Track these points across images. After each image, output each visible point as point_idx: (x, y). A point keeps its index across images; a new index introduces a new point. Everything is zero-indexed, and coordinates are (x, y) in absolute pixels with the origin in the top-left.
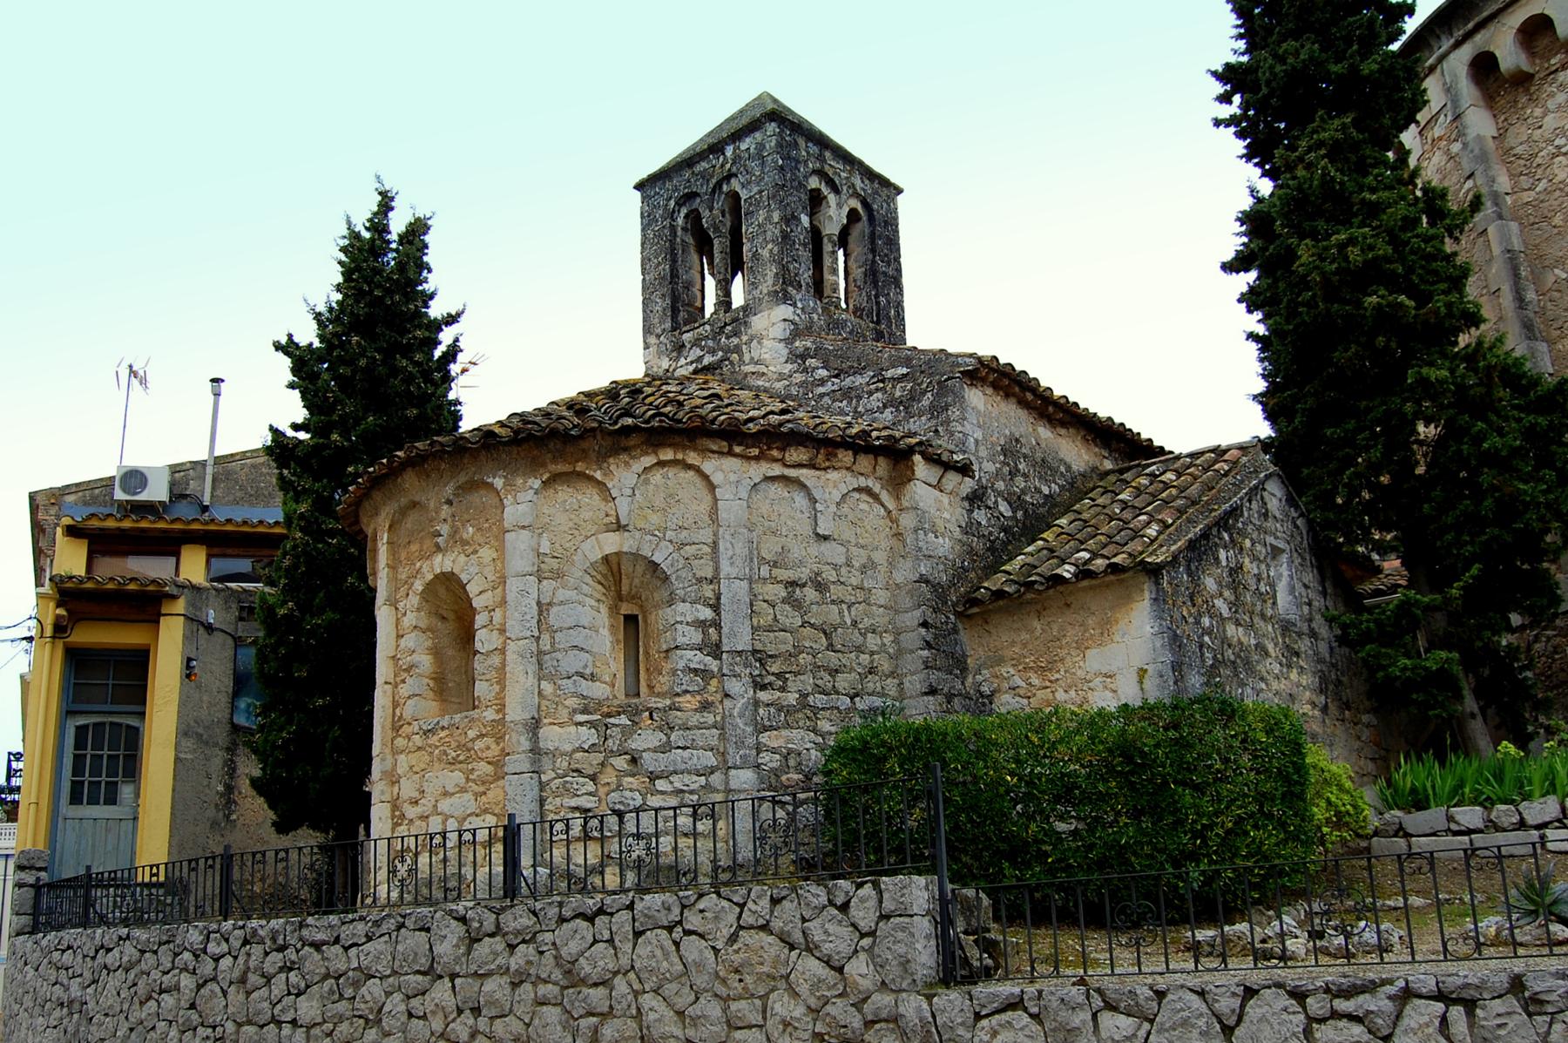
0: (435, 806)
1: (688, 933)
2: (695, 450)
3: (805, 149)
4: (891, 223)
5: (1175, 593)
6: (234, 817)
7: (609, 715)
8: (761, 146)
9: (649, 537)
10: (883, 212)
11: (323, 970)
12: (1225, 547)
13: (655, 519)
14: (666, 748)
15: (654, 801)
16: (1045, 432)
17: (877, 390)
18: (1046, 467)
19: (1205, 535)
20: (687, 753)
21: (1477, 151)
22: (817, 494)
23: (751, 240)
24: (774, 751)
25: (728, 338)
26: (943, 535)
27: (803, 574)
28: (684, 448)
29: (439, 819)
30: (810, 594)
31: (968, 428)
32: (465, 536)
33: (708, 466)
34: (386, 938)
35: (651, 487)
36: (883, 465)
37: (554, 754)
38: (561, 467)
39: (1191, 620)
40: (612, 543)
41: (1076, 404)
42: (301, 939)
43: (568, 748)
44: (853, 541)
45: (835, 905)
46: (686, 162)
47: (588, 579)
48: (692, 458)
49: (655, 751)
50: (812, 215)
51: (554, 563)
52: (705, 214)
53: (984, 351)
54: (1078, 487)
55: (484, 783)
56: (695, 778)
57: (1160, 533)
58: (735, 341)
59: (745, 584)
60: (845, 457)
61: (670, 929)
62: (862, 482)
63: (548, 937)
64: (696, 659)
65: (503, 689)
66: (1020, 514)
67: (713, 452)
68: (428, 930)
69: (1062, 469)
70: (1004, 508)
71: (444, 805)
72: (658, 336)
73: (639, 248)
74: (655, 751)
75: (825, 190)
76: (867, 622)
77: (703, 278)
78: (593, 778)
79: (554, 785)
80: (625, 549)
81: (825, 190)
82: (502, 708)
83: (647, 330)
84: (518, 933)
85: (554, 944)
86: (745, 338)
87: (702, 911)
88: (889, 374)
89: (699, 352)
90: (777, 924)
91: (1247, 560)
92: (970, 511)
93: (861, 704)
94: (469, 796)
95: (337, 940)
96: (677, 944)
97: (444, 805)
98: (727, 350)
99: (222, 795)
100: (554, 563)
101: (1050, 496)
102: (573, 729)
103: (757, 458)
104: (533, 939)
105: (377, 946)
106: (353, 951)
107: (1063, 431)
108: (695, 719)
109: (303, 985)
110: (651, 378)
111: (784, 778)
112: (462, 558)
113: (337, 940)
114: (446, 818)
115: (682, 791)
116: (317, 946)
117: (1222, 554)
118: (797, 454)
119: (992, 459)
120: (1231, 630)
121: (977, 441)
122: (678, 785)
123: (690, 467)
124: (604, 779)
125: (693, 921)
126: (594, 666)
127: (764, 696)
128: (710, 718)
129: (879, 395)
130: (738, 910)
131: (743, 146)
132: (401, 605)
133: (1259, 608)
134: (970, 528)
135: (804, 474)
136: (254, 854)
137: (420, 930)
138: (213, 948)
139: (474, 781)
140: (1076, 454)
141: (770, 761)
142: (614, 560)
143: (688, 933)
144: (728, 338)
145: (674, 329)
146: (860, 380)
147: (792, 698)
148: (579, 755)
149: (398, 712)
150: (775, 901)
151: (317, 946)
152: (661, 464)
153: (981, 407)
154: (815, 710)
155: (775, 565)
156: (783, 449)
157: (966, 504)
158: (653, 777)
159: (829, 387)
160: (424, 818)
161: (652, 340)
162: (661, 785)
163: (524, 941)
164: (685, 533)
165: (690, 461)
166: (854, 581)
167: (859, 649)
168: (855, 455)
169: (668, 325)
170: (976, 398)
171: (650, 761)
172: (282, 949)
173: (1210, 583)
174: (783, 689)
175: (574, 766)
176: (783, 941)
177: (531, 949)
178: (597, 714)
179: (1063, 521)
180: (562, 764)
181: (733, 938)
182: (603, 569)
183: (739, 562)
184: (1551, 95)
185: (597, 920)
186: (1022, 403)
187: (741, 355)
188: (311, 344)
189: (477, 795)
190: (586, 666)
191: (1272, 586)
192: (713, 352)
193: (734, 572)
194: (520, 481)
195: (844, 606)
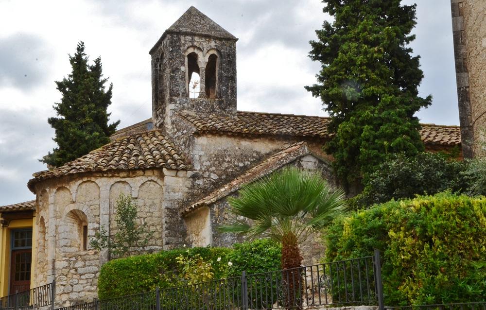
2: (94, 177)
13: (83, 199)
14: (84, 266)
20: (89, 268)
22: (131, 185)
28: (90, 177)
35: (82, 190)
36: (156, 173)
37: (58, 269)
38: (59, 185)
40: (72, 207)
44: (147, 197)
47: (68, 218)
48: (93, 179)
51: (59, 214)
56: (92, 275)
62: (150, 178)
74: (81, 267)
75: (196, 51)
76: (151, 223)
78: (66, 276)
81: (196, 51)
100: (59, 214)
108: (92, 257)
118: (122, 175)
122: (87, 277)
123: (93, 182)
124: (69, 276)
128: (96, 257)
135: (127, 180)
156: (118, 173)
158: (81, 275)
162: (83, 277)
164: (91, 202)
165: (92, 180)
166: (146, 210)
171: (80, 271)
178: (69, 258)
180: (60, 272)
183: (106, 209)
188: (327, 26)
193: (104, 213)
195: (142, 219)
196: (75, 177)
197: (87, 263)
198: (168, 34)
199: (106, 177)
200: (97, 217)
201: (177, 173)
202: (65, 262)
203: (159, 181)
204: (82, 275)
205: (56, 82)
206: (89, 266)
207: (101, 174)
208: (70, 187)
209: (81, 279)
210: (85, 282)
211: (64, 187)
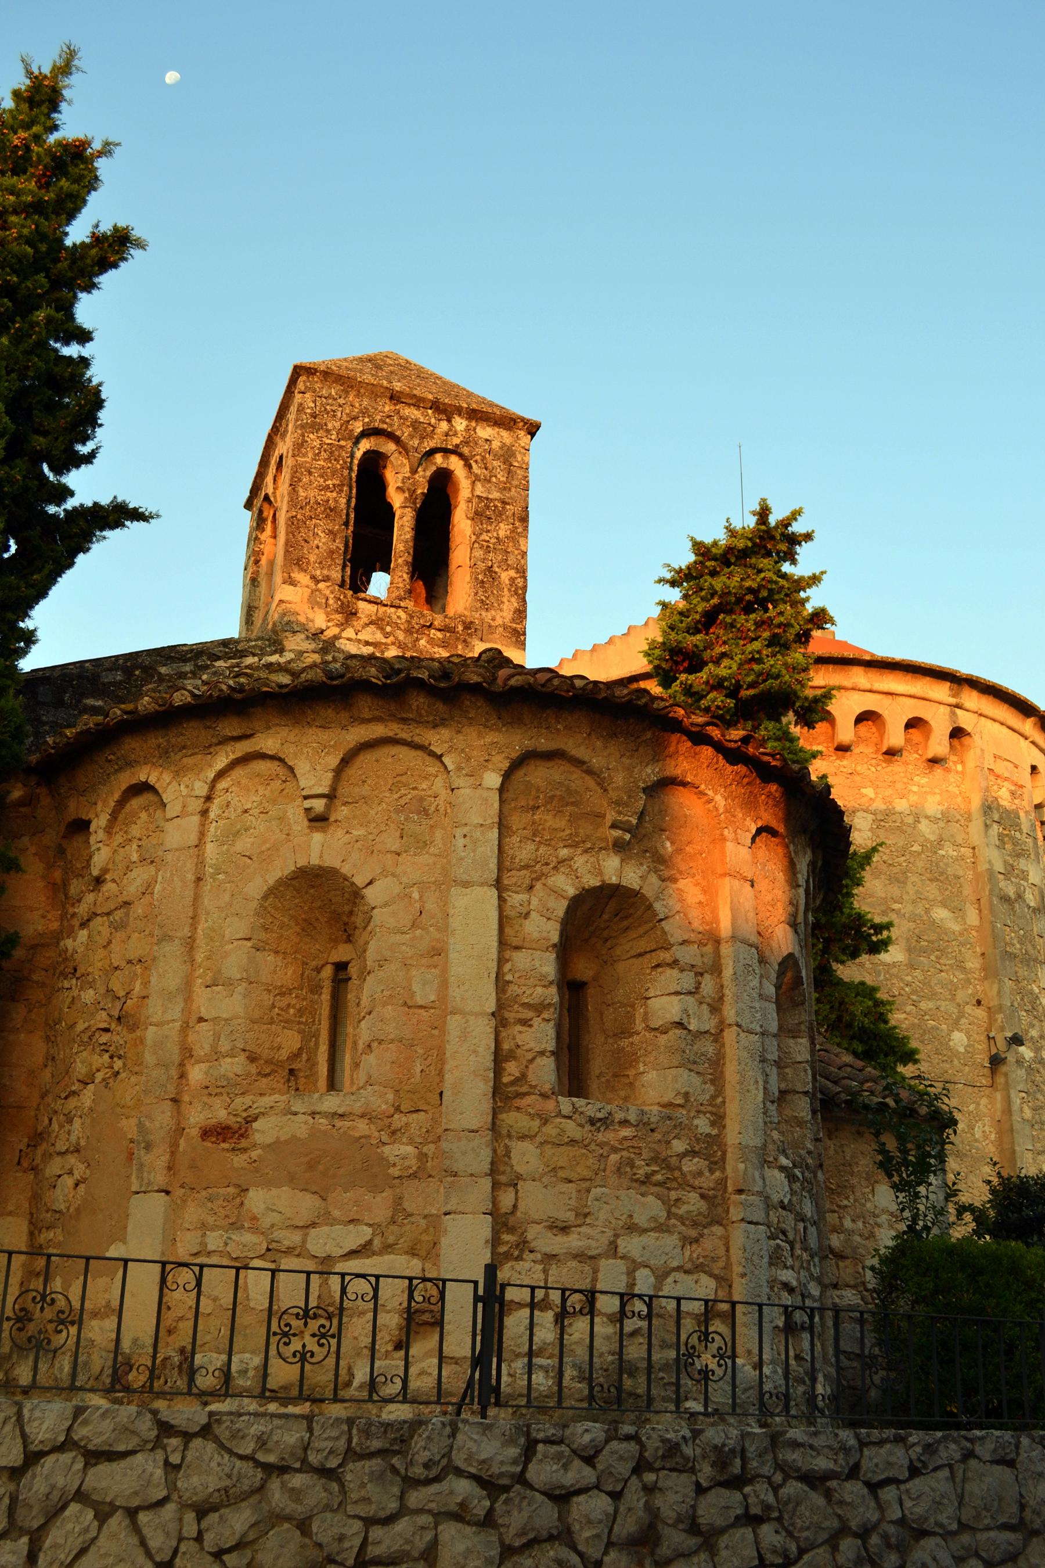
11: (836, 1524)
29: (621, 1266)
34: (945, 1473)
42: (778, 1466)
55: (695, 1224)
68: (1011, 1464)
71: (631, 1245)
82: (718, 1120)
95: (854, 1472)
105: (937, 1483)
106: (889, 1494)
109: (793, 1548)
113: (854, 1472)
114: (633, 1267)
116: (813, 1480)
137: (998, 1462)
138: (544, 1471)
139: (681, 1219)
151: (813, 1480)
172: (737, 1483)
189: (687, 1241)
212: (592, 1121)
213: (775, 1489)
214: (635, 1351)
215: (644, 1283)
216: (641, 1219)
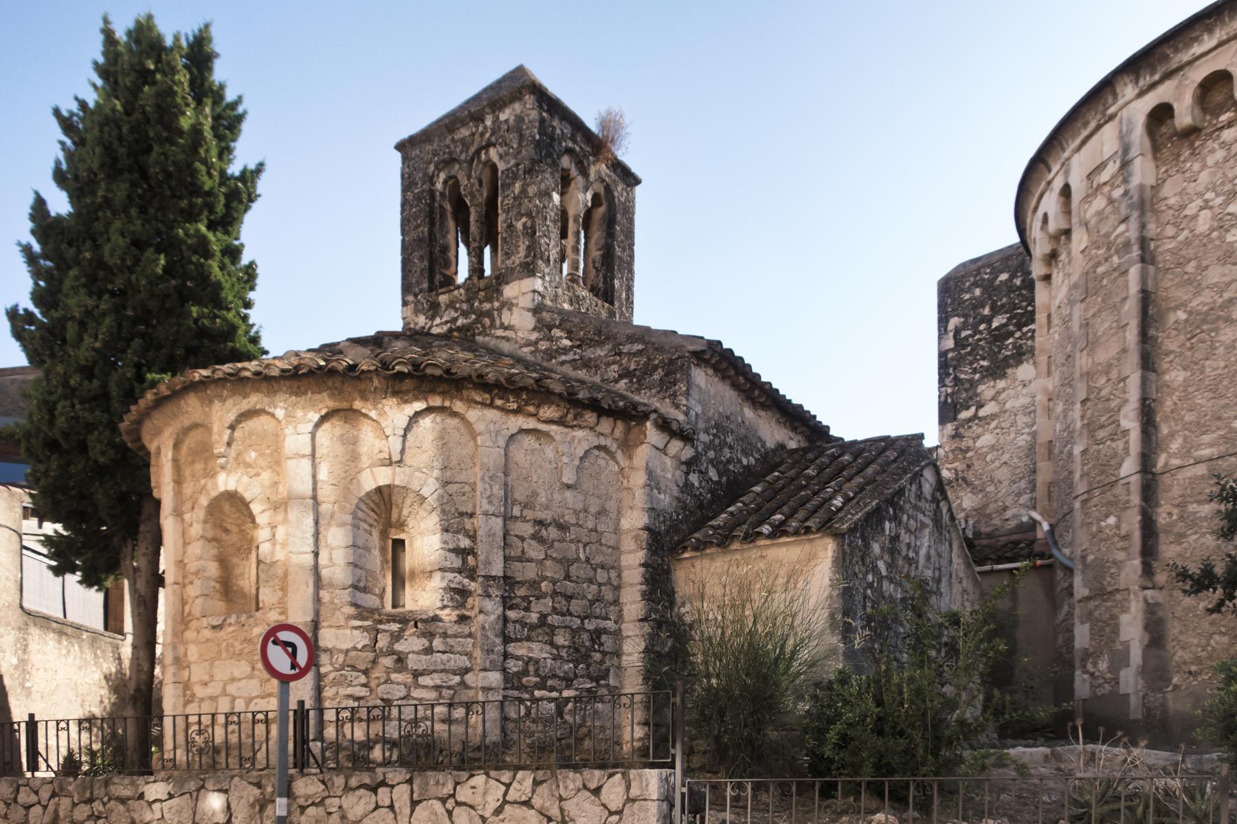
0: (224, 689)
1: (458, 804)
2: (461, 400)
3: (558, 126)
4: (629, 212)
5: (852, 553)
6: (28, 685)
7: (381, 622)
8: (519, 119)
9: (417, 474)
10: (622, 199)
12: (890, 520)
14: (429, 651)
15: (417, 693)
16: (749, 413)
17: (614, 363)
18: (748, 442)
19: (878, 509)
20: (445, 657)
21: (1135, 198)
23: (507, 211)
24: (518, 658)
25: (481, 302)
26: (665, 493)
27: (546, 515)
28: (452, 398)
29: (227, 699)
30: (553, 533)
31: (692, 402)
32: (248, 460)
33: (473, 414)
39: (861, 576)
41: (777, 391)
43: (345, 646)
45: (588, 790)
46: (450, 123)
48: (459, 406)
49: (418, 653)
50: (562, 194)
52: (464, 181)
53: (710, 335)
54: (772, 459)
56: (451, 677)
57: (844, 504)
58: (487, 306)
59: (500, 521)
60: (590, 417)
61: (443, 801)
62: (602, 441)
63: (336, 801)
64: (457, 580)
65: (285, 595)
66: (724, 479)
67: (477, 403)
69: (759, 445)
70: (713, 474)
71: (231, 689)
72: (416, 295)
73: (399, 209)
74: (418, 653)
75: (574, 172)
77: (458, 246)
78: (366, 672)
79: (331, 676)
80: (397, 483)
81: (574, 172)
83: (406, 288)
84: (307, 797)
85: (340, 807)
86: (496, 304)
87: (473, 787)
88: (625, 349)
89: (454, 314)
90: (537, 802)
91: (903, 531)
92: (687, 474)
93: (590, 625)
94: (255, 682)
96: (450, 813)
97: (231, 689)
98: (481, 314)
99: (16, 667)
101: (748, 467)
102: (348, 631)
103: (516, 412)
104: (321, 803)
107: (763, 413)
110: (411, 335)
111: (525, 680)
112: (245, 479)
115: (441, 687)
117: (887, 525)
118: (548, 412)
119: (706, 431)
120: (885, 584)
121: (697, 415)
122: (438, 682)
123: (455, 414)
125: (464, 794)
126: (367, 580)
127: (512, 614)
129: (615, 367)
130: (503, 788)
131: (503, 117)
132: (187, 517)
133: (905, 570)
134: (687, 487)
136: (58, 722)
140: (772, 433)
141: (514, 666)
142: (386, 492)
143: (458, 804)
144: (481, 302)
145: (431, 290)
146: (600, 352)
147: (534, 617)
148: (353, 653)
149: (187, 609)
150: (536, 783)
152: (430, 410)
153: (703, 386)
154: (553, 628)
155: (525, 506)
157: (684, 468)
159: (570, 357)
160: (213, 698)
161: (411, 298)
163: (313, 804)
165: (456, 409)
167: (591, 581)
168: (599, 417)
169: (425, 285)
170: (701, 377)
173: (876, 548)
174: (527, 609)
175: (350, 662)
176: (542, 814)
177: (321, 810)
179: (758, 489)
181: (498, 811)
182: (376, 498)
183: (496, 501)
184: (1213, 151)
185: (380, 790)
186: (735, 386)
187: (493, 321)
190: (359, 581)
191: (917, 553)
192: (465, 314)
194: (300, 413)
195: (581, 545)
196: (404, 388)
197: (437, 643)
198: (533, 93)
199: (498, 408)
200: (466, 520)
201: (303, 456)
202: (356, 632)
203: (619, 455)
204: (422, 675)
205: (37, 193)
206: (444, 652)
207: (487, 396)
208: (382, 413)
209: (417, 686)
210: (431, 695)
211: (358, 413)
212: (214, 627)
213: (104, 804)
214: (234, 739)
215: (240, 706)
216: (237, 674)
